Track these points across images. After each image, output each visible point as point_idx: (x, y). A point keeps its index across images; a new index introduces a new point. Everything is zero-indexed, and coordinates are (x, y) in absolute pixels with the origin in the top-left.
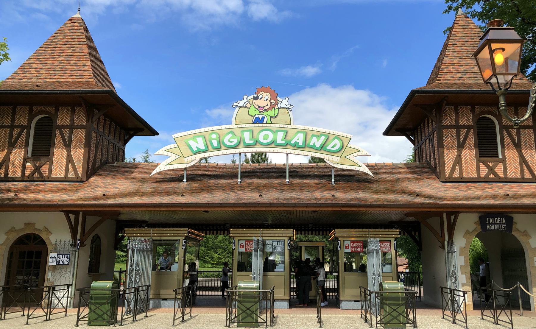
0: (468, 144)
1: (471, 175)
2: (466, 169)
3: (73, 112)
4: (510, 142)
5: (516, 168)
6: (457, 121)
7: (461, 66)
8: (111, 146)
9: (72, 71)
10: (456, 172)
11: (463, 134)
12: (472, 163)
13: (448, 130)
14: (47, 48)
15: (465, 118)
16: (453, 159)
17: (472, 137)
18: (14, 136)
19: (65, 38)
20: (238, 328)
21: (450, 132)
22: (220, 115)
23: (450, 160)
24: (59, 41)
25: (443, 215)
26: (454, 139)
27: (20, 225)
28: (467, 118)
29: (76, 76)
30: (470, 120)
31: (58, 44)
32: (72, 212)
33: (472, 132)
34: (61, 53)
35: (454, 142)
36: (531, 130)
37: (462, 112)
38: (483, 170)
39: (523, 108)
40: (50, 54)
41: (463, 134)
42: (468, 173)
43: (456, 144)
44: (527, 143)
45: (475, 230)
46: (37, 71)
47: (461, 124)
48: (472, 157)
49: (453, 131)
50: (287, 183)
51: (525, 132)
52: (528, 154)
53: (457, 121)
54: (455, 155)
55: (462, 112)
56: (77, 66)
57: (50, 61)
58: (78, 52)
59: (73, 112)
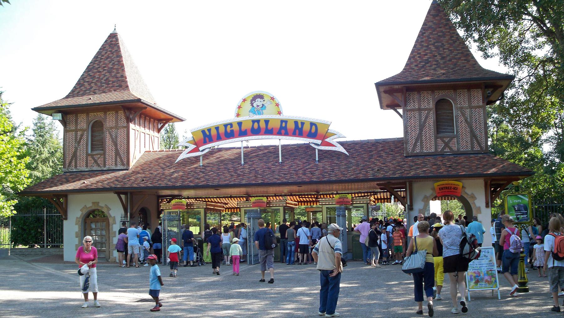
0: (428, 123)
1: (430, 149)
2: (426, 145)
3: (117, 112)
4: (463, 121)
5: (467, 142)
6: (420, 105)
7: (426, 55)
8: (147, 136)
9: (113, 82)
10: (417, 148)
11: (424, 115)
12: (431, 139)
13: (411, 113)
14: (95, 64)
15: (425, 102)
16: (415, 137)
17: (431, 118)
18: (79, 137)
19: (106, 53)
20: (98, 201)
21: (413, 114)
22: (136, 228)
23: (413, 137)
24: (102, 56)
25: (406, 184)
26: (416, 120)
27: (89, 205)
28: (428, 101)
29: (117, 86)
30: (430, 103)
31: (102, 59)
32: (123, 193)
33: (431, 113)
34: (104, 67)
35: (416, 122)
36: (480, 109)
37: (423, 97)
38: (440, 145)
39: (475, 91)
40: (97, 69)
41: (424, 115)
42: (428, 148)
43: (418, 124)
44: (477, 121)
45: (432, 195)
46: (89, 85)
47: (422, 107)
48: (431, 135)
49: (416, 113)
50: (281, 163)
51: (476, 111)
52: (477, 130)
53: (420, 105)
54: (416, 134)
55: (423, 97)
56: (117, 78)
57: (97, 76)
58: (117, 64)
59: (117, 112)
